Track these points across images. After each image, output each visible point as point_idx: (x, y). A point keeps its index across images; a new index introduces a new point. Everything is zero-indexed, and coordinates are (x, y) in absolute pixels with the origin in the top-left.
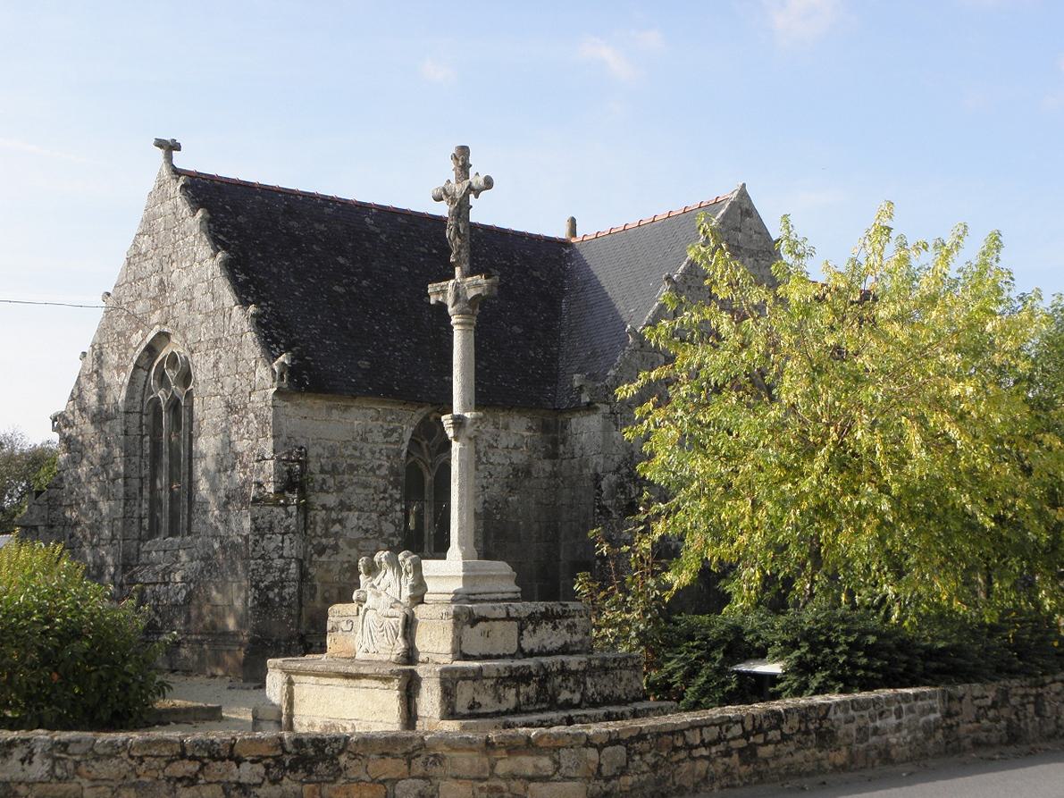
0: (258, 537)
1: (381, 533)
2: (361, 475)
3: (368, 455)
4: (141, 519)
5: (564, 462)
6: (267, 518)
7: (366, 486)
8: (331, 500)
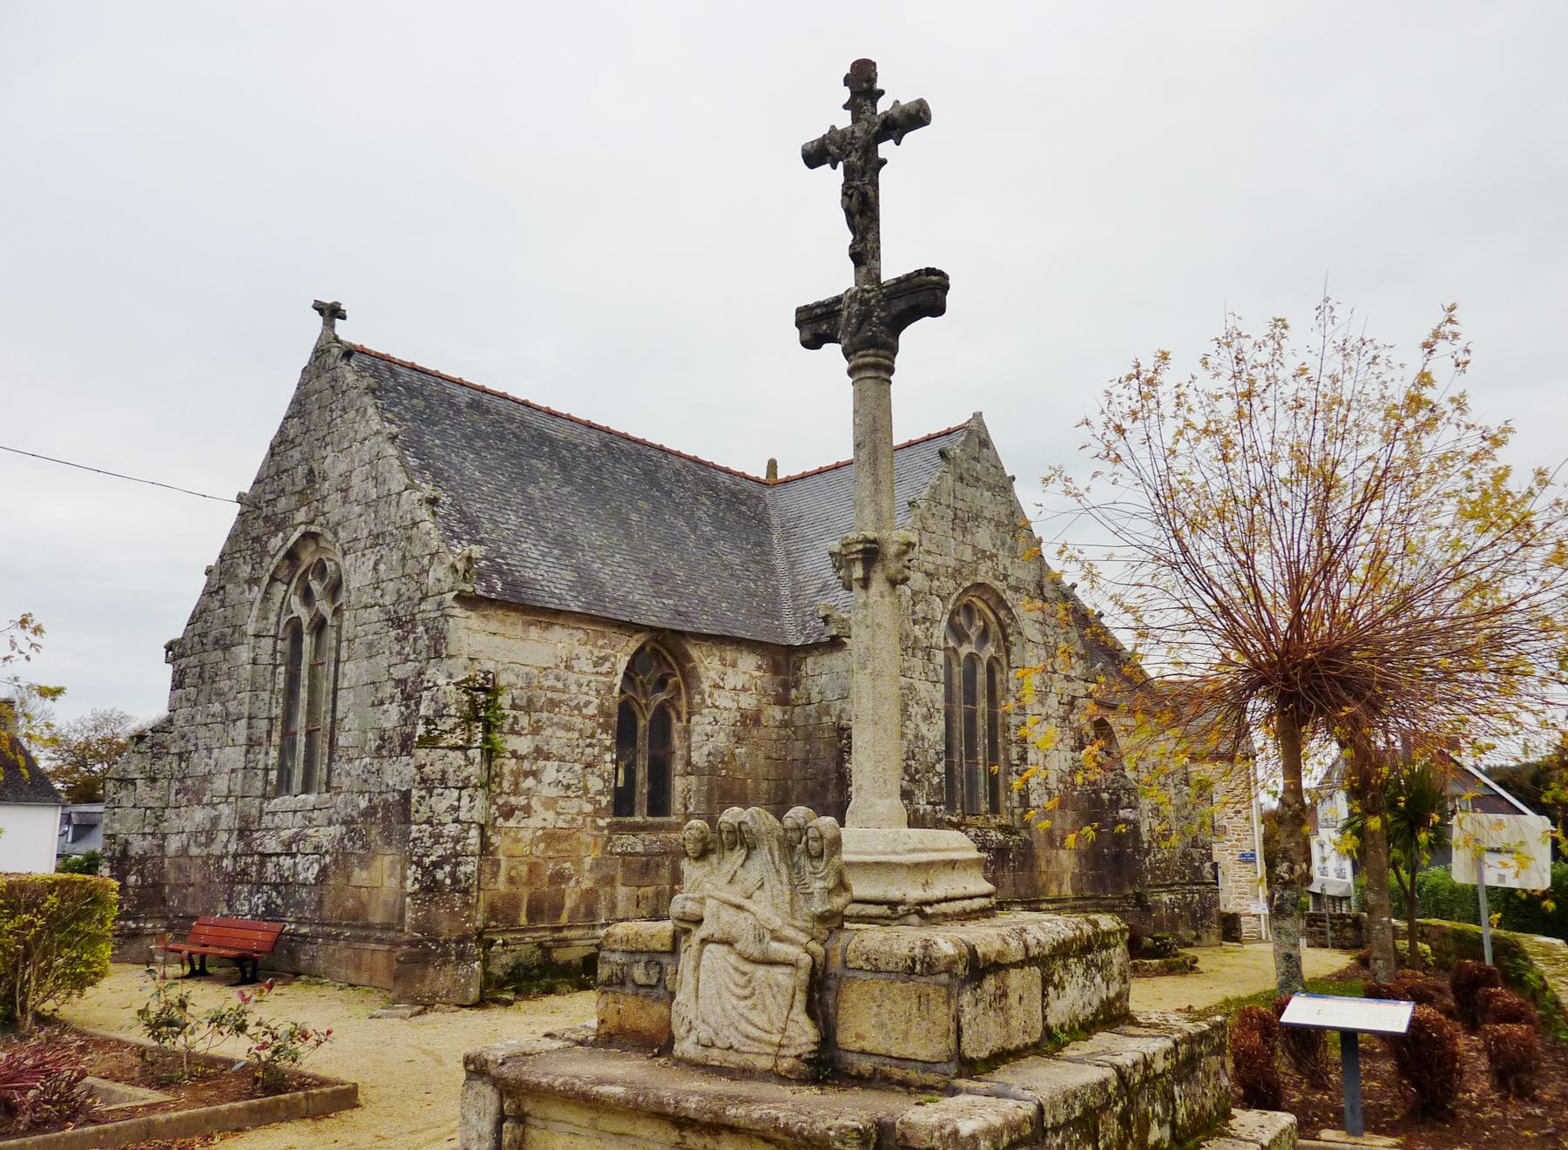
0: (423, 793)
1: (586, 790)
2: (563, 715)
3: (574, 688)
4: (267, 770)
5: (797, 710)
6: (439, 766)
7: (569, 728)
8: (523, 745)
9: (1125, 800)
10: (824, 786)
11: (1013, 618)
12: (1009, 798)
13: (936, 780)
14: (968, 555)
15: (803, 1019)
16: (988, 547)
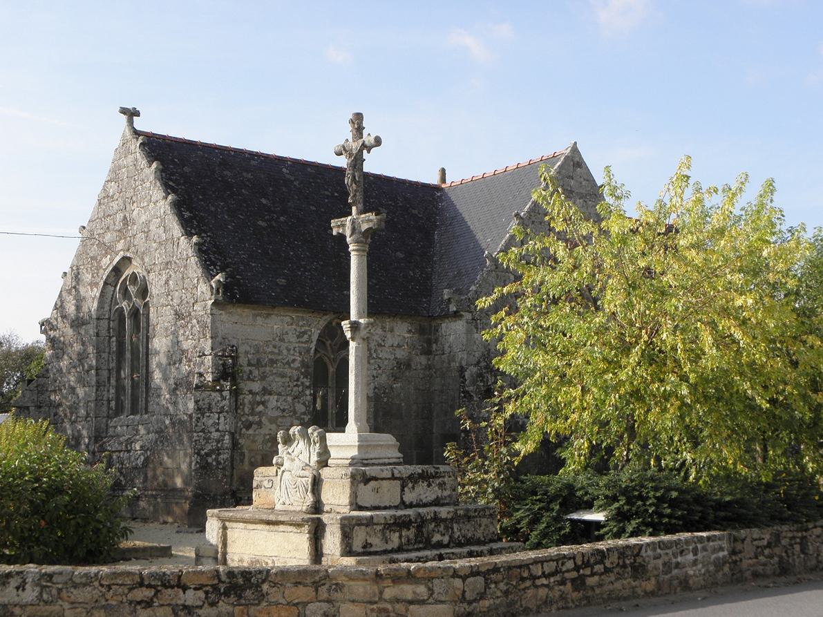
0: (199, 415)
1: (295, 412)
2: (279, 368)
3: (285, 352)
4: (109, 401)
5: (436, 357)
6: (207, 401)
7: (283, 376)
8: (256, 386)
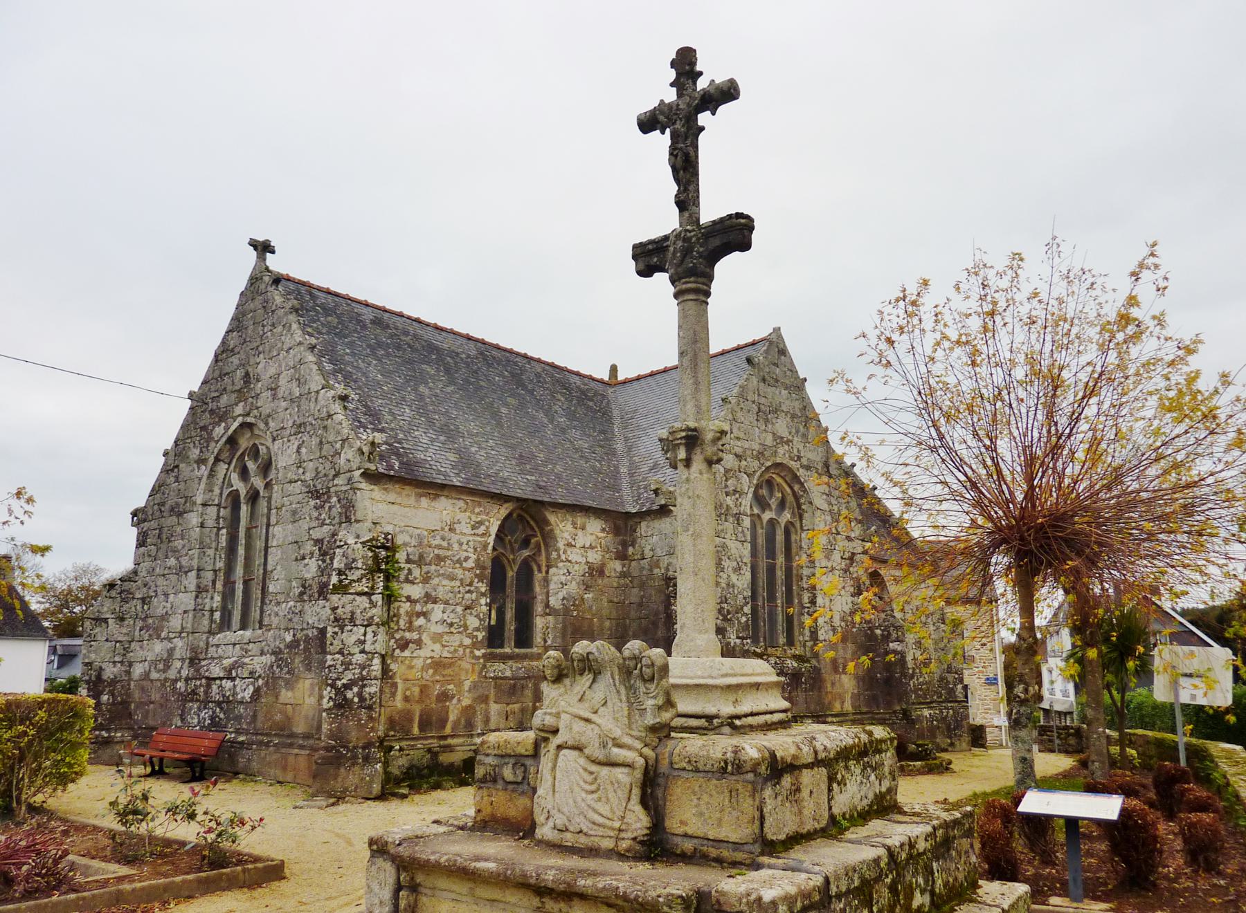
0: (336, 629)
1: (466, 627)
2: (447, 568)
3: (456, 546)
4: (212, 611)
5: (633, 563)
6: (349, 608)
7: (452, 578)
8: (416, 591)
9: (894, 635)
10: (655, 624)
11: (805, 491)
12: (802, 634)
13: (744, 619)
14: (769, 440)
15: (638, 809)
16: (785, 434)
